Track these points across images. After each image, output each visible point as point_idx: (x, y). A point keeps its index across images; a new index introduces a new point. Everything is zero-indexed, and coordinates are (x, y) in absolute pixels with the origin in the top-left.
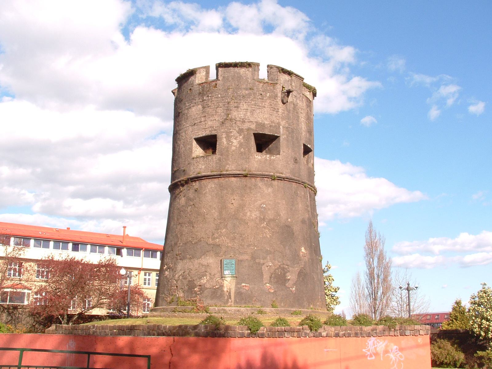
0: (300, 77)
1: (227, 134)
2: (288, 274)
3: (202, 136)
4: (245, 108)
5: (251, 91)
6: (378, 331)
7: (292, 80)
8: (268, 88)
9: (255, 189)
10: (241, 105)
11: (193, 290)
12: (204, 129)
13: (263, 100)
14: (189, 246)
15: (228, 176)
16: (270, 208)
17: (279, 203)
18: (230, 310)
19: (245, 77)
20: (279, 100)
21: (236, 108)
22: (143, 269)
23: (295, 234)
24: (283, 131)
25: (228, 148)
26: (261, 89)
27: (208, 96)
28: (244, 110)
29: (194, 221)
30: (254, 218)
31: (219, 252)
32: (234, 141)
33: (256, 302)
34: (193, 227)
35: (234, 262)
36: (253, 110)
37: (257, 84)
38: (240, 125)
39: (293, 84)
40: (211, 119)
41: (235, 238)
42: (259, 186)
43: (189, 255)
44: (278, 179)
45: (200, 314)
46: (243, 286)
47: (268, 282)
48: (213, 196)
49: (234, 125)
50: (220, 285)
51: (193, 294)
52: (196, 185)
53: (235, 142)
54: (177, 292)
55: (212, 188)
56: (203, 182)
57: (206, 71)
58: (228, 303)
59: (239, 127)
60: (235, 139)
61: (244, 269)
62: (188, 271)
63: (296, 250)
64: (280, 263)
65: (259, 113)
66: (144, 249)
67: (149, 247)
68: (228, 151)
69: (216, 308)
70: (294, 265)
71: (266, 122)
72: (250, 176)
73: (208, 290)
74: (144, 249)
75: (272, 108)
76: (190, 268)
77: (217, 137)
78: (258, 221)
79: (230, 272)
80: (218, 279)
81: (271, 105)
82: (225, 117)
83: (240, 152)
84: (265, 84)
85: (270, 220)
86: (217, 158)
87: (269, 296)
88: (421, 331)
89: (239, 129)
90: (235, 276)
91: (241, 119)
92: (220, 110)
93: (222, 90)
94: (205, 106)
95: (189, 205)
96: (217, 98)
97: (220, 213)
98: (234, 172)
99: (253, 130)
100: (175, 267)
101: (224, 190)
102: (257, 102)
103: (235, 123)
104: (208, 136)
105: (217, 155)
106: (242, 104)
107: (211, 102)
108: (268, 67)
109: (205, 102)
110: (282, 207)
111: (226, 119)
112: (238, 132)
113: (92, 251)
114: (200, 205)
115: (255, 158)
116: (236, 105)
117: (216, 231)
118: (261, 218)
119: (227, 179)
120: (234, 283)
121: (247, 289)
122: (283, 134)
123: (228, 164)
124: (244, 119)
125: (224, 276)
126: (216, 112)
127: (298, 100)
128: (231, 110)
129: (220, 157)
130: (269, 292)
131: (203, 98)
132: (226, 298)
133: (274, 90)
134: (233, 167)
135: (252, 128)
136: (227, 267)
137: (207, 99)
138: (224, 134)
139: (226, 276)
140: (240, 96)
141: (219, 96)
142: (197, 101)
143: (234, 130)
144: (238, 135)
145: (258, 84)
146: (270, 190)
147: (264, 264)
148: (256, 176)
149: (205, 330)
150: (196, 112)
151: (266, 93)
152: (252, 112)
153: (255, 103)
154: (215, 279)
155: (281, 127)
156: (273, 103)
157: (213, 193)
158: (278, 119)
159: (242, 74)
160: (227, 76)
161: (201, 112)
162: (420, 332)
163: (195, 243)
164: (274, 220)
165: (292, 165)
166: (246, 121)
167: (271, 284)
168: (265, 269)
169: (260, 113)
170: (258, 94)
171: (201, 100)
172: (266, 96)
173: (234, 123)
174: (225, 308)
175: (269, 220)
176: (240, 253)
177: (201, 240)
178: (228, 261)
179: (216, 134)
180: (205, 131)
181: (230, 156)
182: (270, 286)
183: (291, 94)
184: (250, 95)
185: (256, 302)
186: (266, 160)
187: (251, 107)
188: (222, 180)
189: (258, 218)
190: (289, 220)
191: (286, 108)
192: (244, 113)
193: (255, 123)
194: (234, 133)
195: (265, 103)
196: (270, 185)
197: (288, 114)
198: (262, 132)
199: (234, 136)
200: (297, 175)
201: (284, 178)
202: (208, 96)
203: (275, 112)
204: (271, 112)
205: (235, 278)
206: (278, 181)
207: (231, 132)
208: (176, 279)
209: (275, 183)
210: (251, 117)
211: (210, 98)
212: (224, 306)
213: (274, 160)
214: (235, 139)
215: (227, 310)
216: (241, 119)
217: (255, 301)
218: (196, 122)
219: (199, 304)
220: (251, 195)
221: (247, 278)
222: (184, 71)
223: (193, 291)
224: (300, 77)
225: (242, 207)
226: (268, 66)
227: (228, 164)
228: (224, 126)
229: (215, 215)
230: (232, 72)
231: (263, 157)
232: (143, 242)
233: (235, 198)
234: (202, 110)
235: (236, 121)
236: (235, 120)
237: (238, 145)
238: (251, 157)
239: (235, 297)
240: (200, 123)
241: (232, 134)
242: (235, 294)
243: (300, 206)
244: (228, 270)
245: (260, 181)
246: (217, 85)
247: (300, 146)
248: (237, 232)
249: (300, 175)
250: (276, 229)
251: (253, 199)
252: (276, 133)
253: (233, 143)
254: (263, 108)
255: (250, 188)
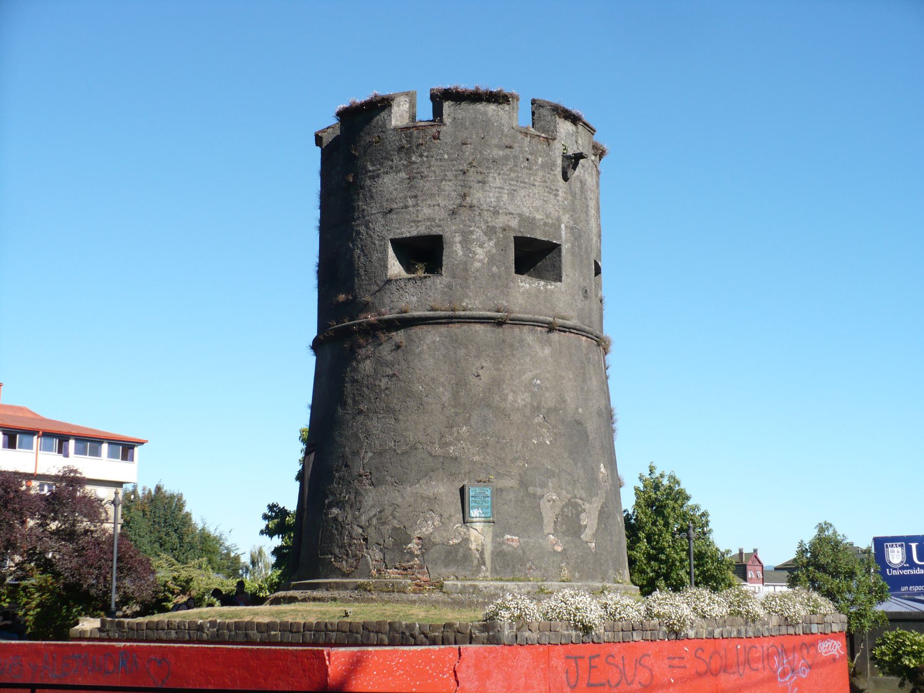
0: (590, 128)
1: (463, 236)
2: (583, 516)
3: (408, 236)
4: (499, 185)
5: (508, 151)
6: (771, 626)
7: (577, 132)
8: (540, 147)
9: (521, 348)
10: (490, 179)
11: (404, 547)
12: (414, 221)
13: (531, 172)
14: (390, 459)
15: (468, 320)
16: (549, 386)
17: (562, 376)
18: (486, 588)
19: (497, 122)
20: (558, 170)
21: (481, 184)
22: (39, 475)
23: (590, 438)
24: (566, 234)
25: (465, 263)
26: (527, 149)
27: (421, 156)
28: (497, 190)
29: (397, 408)
30: (520, 405)
31: (458, 472)
32: (479, 250)
33: (532, 570)
34: (396, 420)
35: (489, 493)
36: (514, 190)
37: (520, 138)
38: (489, 220)
39: (580, 142)
40: (429, 202)
41: (487, 445)
42: (528, 344)
43: (391, 477)
44: (511, 324)
45: (426, 595)
46: (508, 540)
47: (553, 532)
48: (438, 359)
49: (477, 218)
50: (462, 538)
51: (405, 555)
52: (399, 336)
53: (480, 253)
54: (365, 550)
55: (434, 342)
56: (414, 331)
57: (410, 102)
58: (480, 573)
59: (488, 222)
60: (481, 246)
61: (507, 506)
62: (391, 509)
63: (592, 469)
64: (570, 493)
65: (525, 196)
66: (41, 432)
67: (10, 424)
68: (466, 270)
69: (459, 584)
70: (592, 498)
71: (538, 217)
72: (512, 322)
73: (438, 547)
74: (41, 432)
75: (547, 187)
76: (395, 502)
77: (443, 240)
78: (528, 411)
79: (481, 511)
80: (457, 525)
81: (545, 182)
82: (458, 202)
83: (490, 274)
84: (533, 138)
85: (549, 411)
86: (444, 282)
87: (555, 559)
88: (833, 624)
89: (488, 227)
90: (491, 519)
91: (490, 206)
92: (448, 186)
93: (451, 145)
94: (415, 175)
95: (384, 374)
96: (441, 160)
97: (455, 395)
98: (481, 313)
99: (514, 230)
100: (357, 499)
101: (461, 349)
102: (520, 175)
103: (480, 214)
104: (425, 236)
105: (444, 278)
106: (492, 177)
107: (429, 167)
108: (532, 104)
109: (416, 166)
110: (568, 384)
111: (461, 206)
112: (486, 234)
113: (77, 452)
114: (410, 376)
115: (519, 286)
116: (480, 178)
117: (447, 430)
118: (534, 407)
119: (465, 327)
120: (490, 535)
121: (516, 546)
122: (567, 241)
123: (467, 296)
124: (497, 208)
125: (470, 519)
126: (440, 190)
127: (586, 173)
128: (470, 187)
129: (450, 282)
130: (555, 551)
131: (410, 158)
132: (475, 562)
133: (550, 153)
134: (477, 302)
135: (513, 226)
136: (475, 502)
137: (418, 161)
138: (457, 234)
139: (475, 520)
140: (488, 160)
141: (446, 157)
142: (395, 162)
143: (478, 227)
144: (486, 238)
145: (522, 138)
146: (547, 351)
147: (543, 495)
148: (522, 323)
149: (509, 631)
150: (394, 186)
151: (536, 156)
152: (512, 194)
153: (518, 177)
154: (451, 525)
155: (563, 226)
156: (549, 177)
157: (437, 353)
158: (557, 211)
159: (492, 117)
160: (460, 117)
161: (404, 186)
162: (833, 627)
163: (403, 453)
164: (555, 410)
165: (580, 303)
166: (501, 211)
167: (557, 536)
168: (545, 506)
169: (527, 197)
170: (523, 157)
171: (405, 163)
172: (536, 163)
173: (477, 214)
174: (477, 583)
175: (548, 409)
176: (499, 474)
177: (416, 446)
178: (477, 489)
179: (441, 233)
180: (418, 227)
181: (470, 281)
182: (556, 539)
183: (581, 161)
184: (506, 158)
185: (532, 570)
186: (539, 290)
187: (510, 184)
188: (455, 329)
189: (529, 406)
190: (580, 409)
191: (570, 188)
192: (497, 194)
193: (517, 216)
194: (478, 234)
195: (535, 177)
196: (546, 341)
197: (573, 202)
198: (530, 234)
199: (477, 240)
200: (587, 322)
201: (569, 328)
202: (421, 156)
203: (552, 197)
204: (546, 196)
205: (492, 524)
206: (559, 334)
207: (472, 232)
208: (363, 524)
209: (555, 336)
210: (509, 203)
211: (425, 159)
212: (472, 580)
213: (552, 292)
214: (480, 247)
215: (481, 586)
216: (490, 206)
217: (531, 568)
218: (395, 206)
219: (419, 576)
220: (513, 360)
221: (514, 524)
222: (361, 97)
223: (405, 549)
224: (590, 128)
225: (497, 383)
226: (533, 102)
227: (467, 296)
228: (457, 219)
229: (445, 399)
230: (471, 111)
231: (533, 285)
232: (33, 416)
233: (484, 364)
234: (409, 183)
235: (481, 210)
236: (479, 207)
237: (487, 259)
238: (512, 284)
239: (493, 561)
240: (404, 210)
241: (474, 237)
242: (492, 554)
243: (595, 383)
244: (478, 508)
245: (529, 332)
246: (441, 135)
247: (590, 264)
248: (491, 433)
249: (591, 322)
250: (560, 427)
251: (518, 368)
252: (555, 238)
253: (476, 255)
254: (532, 187)
255: (511, 346)
